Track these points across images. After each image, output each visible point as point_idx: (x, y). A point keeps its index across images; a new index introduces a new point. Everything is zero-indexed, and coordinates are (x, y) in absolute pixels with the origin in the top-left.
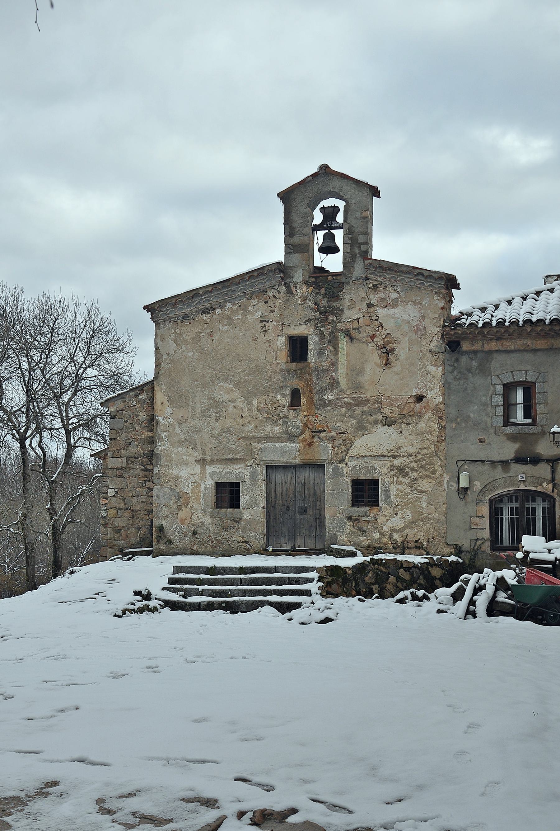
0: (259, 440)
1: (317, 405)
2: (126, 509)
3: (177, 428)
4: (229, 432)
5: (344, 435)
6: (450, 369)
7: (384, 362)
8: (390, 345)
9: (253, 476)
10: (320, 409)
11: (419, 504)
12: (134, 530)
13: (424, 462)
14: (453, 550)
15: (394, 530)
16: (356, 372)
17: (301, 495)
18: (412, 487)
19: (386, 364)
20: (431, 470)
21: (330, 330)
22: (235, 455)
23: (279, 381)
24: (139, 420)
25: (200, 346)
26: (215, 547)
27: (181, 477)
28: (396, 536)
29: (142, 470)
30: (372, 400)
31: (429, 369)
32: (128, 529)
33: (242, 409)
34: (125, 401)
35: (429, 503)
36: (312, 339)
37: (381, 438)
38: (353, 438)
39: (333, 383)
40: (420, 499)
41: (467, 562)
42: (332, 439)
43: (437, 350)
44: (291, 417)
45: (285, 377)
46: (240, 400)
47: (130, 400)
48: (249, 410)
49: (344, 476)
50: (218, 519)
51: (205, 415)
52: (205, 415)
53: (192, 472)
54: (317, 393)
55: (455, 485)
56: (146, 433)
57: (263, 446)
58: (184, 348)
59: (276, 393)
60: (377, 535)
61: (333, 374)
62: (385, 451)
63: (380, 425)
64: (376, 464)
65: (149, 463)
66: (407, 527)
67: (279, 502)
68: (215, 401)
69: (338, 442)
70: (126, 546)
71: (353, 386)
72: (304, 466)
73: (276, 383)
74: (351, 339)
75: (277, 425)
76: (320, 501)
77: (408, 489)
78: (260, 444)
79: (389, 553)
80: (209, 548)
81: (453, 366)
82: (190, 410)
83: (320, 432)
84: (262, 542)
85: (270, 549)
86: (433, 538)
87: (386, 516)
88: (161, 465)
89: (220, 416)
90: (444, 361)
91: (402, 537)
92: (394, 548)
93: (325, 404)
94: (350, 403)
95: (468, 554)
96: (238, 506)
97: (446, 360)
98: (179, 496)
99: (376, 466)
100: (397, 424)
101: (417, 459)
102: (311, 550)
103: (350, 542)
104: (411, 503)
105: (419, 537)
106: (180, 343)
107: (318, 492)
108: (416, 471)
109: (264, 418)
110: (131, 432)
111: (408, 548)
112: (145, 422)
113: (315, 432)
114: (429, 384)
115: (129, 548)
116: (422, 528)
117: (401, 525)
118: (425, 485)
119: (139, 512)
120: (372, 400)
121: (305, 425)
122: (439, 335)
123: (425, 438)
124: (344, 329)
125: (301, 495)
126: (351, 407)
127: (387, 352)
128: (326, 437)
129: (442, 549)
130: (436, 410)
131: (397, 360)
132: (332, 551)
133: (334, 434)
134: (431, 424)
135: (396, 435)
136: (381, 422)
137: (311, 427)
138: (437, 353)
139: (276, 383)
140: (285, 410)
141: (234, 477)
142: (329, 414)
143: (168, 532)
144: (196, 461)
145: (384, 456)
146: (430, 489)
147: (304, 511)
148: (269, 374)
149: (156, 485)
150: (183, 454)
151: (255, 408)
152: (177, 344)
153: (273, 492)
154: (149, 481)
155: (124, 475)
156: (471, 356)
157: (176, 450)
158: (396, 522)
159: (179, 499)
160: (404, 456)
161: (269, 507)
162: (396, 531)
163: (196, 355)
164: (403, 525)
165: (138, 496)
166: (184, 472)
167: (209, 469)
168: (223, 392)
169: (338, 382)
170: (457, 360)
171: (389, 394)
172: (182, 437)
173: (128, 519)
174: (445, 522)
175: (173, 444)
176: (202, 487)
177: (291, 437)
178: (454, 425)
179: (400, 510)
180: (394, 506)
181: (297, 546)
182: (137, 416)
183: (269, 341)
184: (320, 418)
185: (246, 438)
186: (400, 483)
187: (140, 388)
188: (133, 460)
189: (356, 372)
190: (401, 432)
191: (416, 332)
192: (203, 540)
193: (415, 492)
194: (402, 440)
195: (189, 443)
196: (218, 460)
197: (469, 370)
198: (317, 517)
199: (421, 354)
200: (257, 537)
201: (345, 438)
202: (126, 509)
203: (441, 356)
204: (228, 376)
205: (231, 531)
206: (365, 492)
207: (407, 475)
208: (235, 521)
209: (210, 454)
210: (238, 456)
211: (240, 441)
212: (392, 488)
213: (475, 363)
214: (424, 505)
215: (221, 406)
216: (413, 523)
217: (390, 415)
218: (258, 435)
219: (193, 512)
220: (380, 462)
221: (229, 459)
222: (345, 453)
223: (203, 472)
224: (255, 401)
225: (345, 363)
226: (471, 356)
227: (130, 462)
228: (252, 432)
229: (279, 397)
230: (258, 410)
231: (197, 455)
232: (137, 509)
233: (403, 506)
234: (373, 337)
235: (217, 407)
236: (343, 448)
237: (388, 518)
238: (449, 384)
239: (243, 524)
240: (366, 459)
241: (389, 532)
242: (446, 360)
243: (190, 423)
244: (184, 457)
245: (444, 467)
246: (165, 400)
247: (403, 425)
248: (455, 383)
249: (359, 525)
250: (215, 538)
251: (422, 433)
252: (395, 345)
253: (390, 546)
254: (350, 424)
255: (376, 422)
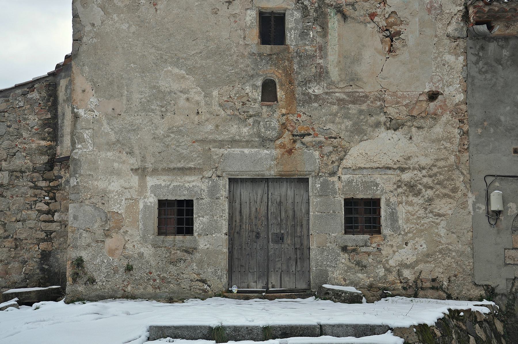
0: (221, 144)
1: (300, 101)
2: (7, 237)
3: (105, 125)
4: (179, 132)
5: (335, 141)
6: (474, 59)
7: (387, 49)
8: (395, 27)
9: (213, 191)
10: (303, 105)
11: (436, 231)
12: (17, 265)
13: (442, 177)
14: (483, 292)
15: (403, 265)
16: (350, 60)
17: (276, 218)
18: (426, 209)
19: (390, 51)
20: (450, 187)
21: (316, 5)
22: (188, 163)
23: (249, 69)
24: (28, 124)
25: (139, 17)
26: (159, 288)
27: (110, 192)
28: (407, 273)
29: (31, 187)
30: (372, 96)
31: (447, 59)
32: (8, 263)
33: (198, 103)
34: (8, 101)
35: (450, 231)
36: (292, 15)
37: (383, 147)
38: (347, 145)
39: (321, 73)
40: (438, 224)
41: (504, 309)
42: (320, 145)
43: (456, 34)
44: (265, 116)
45: (256, 64)
46: (194, 90)
47: (16, 99)
48: (207, 104)
49: (336, 193)
50: (163, 249)
51: (145, 108)
52: (145, 108)
53: (126, 185)
54: (299, 85)
55: (484, 207)
56: (38, 142)
57: (226, 152)
58: (116, 19)
59: (244, 84)
60: (381, 272)
61: (321, 61)
62: (390, 162)
63: (383, 129)
64: (378, 178)
65: (41, 179)
66: (421, 261)
67: (246, 227)
68: (160, 91)
69: (327, 149)
70: (4, 285)
71: (348, 78)
72: (279, 180)
73: (244, 71)
74: (345, 17)
75: (246, 126)
76: (302, 226)
77: (421, 212)
78: (222, 150)
79: (399, 295)
80: (150, 289)
81: (478, 55)
82: (125, 102)
83: (303, 136)
84: (225, 280)
85: (235, 289)
86: (455, 276)
87: (392, 246)
88: (81, 175)
89: (167, 110)
90: (465, 48)
91: (414, 273)
92: (404, 288)
93: (309, 99)
94: (342, 100)
95: (504, 298)
96: (190, 231)
97: (468, 48)
98: (106, 217)
99: (378, 181)
100: (405, 128)
101: (431, 172)
102: (291, 291)
103: (345, 280)
104: (426, 230)
105: (437, 274)
106: (110, 11)
107: (298, 214)
108: (431, 188)
109: (228, 115)
110: (16, 139)
111: (422, 289)
112: (36, 127)
113: (296, 135)
114: (446, 77)
115: (9, 288)
116: (441, 262)
117: (411, 259)
118: (443, 206)
119: (24, 241)
120: (372, 96)
121: (284, 126)
122: (459, 16)
123: (442, 147)
124: (334, 4)
125: (276, 218)
126: (344, 104)
127: (391, 36)
128: (311, 142)
129: (469, 290)
130: (456, 111)
131: (404, 46)
132: (328, 293)
133: (321, 138)
134: (450, 129)
135: (404, 142)
136: (385, 124)
137: (291, 129)
138: (456, 39)
139: (244, 71)
140: (257, 105)
141: (186, 192)
142: (316, 112)
143: (89, 267)
144: (132, 170)
145: (389, 168)
146: (450, 212)
147: (280, 239)
148: (235, 58)
149: (73, 201)
150: (114, 161)
151: (215, 102)
152: (106, 13)
153: (238, 213)
154: (41, 202)
155: (5, 194)
156: (500, 43)
157: (103, 155)
158: (407, 255)
159: (106, 222)
160: (414, 169)
161: (233, 234)
162: (407, 266)
163: (133, 29)
164: (414, 258)
165: (24, 221)
166: (115, 185)
167: (151, 181)
168: (171, 79)
169: (327, 72)
170: (482, 48)
171: (393, 89)
172: (113, 137)
173: (9, 251)
174: (471, 256)
175: (98, 147)
176: (141, 206)
177: (264, 142)
178: (480, 131)
179: (411, 239)
180: (403, 233)
181: (270, 286)
182: (25, 119)
183: (234, 15)
184: (304, 117)
185: (203, 141)
186: (411, 204)
187: (30, 85)
188: (19, 174)
189: (350, 60)
190: (411, 138)
191: (429, 11)
192: (141, 277)
193: (431, 215)
194: (411, 149)
195: (121, 144)
196: (164, 170)
197: (498, 61)
198: (298, 246)
199: (436, 39)
200: (217, 274)
201: (336, 144)
202: (7, 237)
203: (461, 43)
204: (178, 59)
205: (182, 265)
206: (363, 215)
207: (420, 193)
208: (186, 251)
209: (153, 161)
210: (191, 165)
211: (195, 144)
212: (400, 211)
213: (506, 53)
214: (443, 232)
215: (168, 98)
216: (428, 255)
217: (396, 116)
218: (219, 138)
219: (127, 239)
220: (383, 176)
221: (179, 169)
222: (336, 164)
223: (143, 185)
224: (215, 93)
225: (337, 48)
226: (500, 43)
227: (13, 177)
228: (211, 133)
229: (248, 89)
230: (220, 105)
231: (134, 162)
232: (22, 237)
233: (415, 234)
234: (372, 16)
235: (162, 99)
236: (334, 157)
237: (395, 249)
238: (473, 78)
239: (198, 256)
240: (365, 172)
241: (398, 268)
242: (468, 48)
243: (124, 119)
244: (116, 165)
245: (469, 184)
246: (88, 86)
247: (414, 129)
248: (480, 77)
249: (357, 258)
250: (159, 275)
251: (438, 140)
252: (401, 27)
253: (399, 286)
254: (343, 127)
255: (377, 125)
